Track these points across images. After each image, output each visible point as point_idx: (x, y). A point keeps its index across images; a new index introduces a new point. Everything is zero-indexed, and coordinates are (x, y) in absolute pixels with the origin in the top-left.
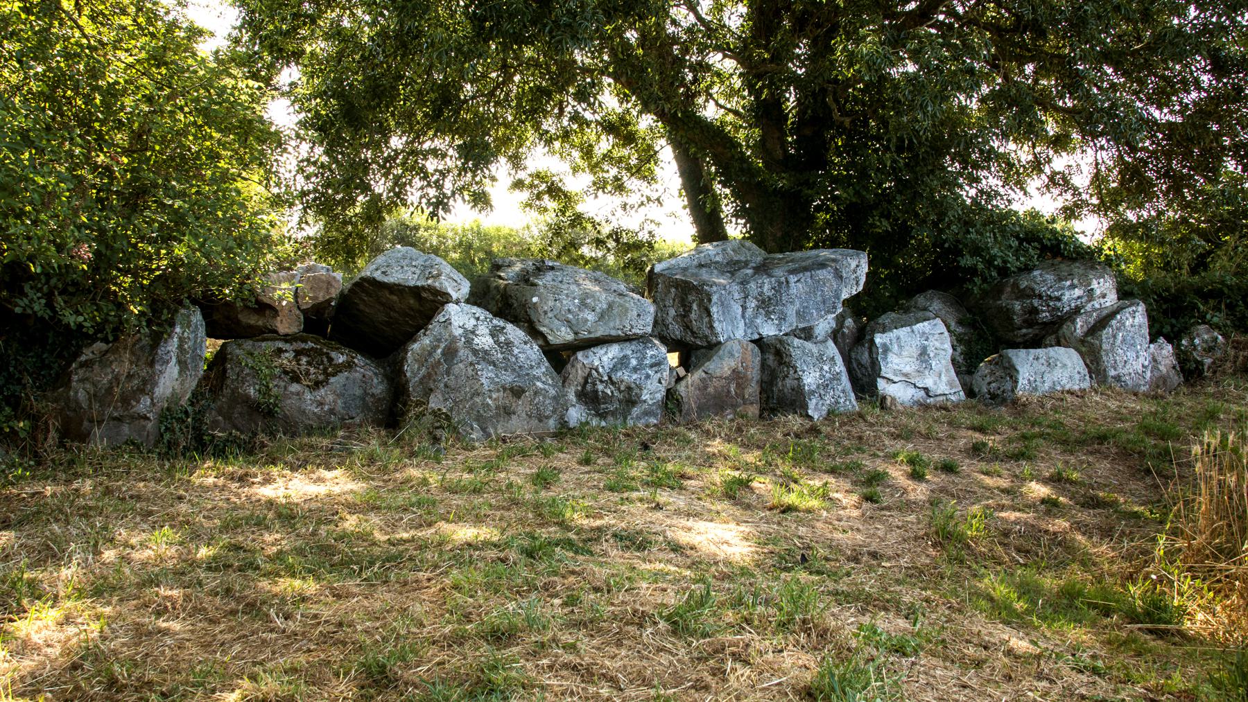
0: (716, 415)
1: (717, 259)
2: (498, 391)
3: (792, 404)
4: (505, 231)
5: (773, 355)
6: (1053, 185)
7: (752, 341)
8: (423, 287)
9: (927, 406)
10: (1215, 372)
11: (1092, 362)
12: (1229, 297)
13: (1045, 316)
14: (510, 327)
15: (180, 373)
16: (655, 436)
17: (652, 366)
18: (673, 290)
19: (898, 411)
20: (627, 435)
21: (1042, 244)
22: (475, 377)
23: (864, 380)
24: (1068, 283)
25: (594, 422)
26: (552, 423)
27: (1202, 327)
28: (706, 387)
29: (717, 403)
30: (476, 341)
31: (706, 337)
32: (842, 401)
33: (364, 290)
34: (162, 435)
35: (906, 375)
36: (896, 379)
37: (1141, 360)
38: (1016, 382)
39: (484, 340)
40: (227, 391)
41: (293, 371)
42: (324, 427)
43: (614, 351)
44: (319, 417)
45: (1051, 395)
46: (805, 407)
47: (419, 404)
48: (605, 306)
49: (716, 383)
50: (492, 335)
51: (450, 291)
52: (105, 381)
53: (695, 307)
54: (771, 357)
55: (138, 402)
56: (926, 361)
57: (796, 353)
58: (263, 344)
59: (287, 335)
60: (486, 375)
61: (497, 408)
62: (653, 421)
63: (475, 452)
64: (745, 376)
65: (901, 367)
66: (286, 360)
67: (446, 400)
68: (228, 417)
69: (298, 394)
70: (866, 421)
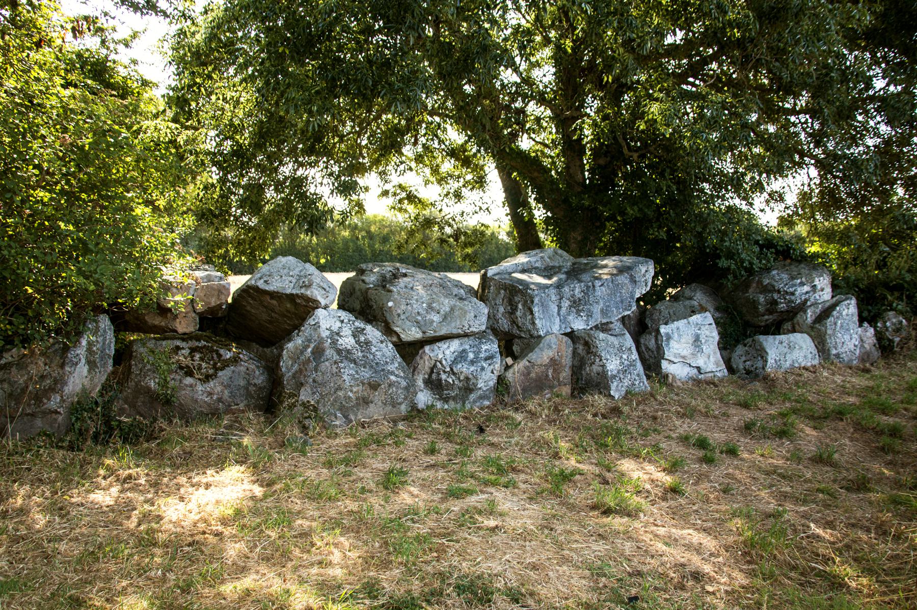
0: (536, 394)
1: (537, 265)
2: (358, 385)
3: (597, 386)
4: (380, 218)
5: (582, 345)
6: (776, 202)
7: (565, 334)
8: (297, 295)
9: (700, 383)
10: (902, 348)
11: (819, 343)
12: (908, 290)
13: (782, 306)
14: (369, 328)
15: (89, 371)
16: (488, 419)
17: (486, 359)
18: (502, 291)
19: (678, 387)
20: (465, 418)
21: (776, 249)
22: (339, 374)
23: (652, 362)
24: (799, 281)
25: (439, 405)
26: (403, 408)
27: (891, 313)
28: (529, 374)
29: (537, 384)
30: (341, 341)
31: (529, 331)
32: (637, 383)
33: (250, 295)
34: (73, 425)
35: (683, 357)
36: (676, 361)
37: (854, 340)
38: (766, 361)
39: (347, 341)
40: (132, 384)
41: (188, 367)
42: (212, 414)
43: (455, 346)
44: (209, 405)
45: (791, 371)
46: (608, 388)
47: (292, 395)
48: (448, 309)
49: (537, 369)
50: (354, 336)
51: (319, 298)
52: (21, 381)
53: (520, 306)
54: (581, 347)
55: (49, 399)
56: (699, 346)
57: (601, 345)
58: (164, 343)
59: (185, 334)
60: (348, 372)
61: (357, 399)
62: (487, 403)
63: (337, 441)
64: (560, 363)
65: (680, 351)
66: (182, 357)
67: (314, 393)
68: (133, 405)
69: (191, 386)
70: (656, 400)
